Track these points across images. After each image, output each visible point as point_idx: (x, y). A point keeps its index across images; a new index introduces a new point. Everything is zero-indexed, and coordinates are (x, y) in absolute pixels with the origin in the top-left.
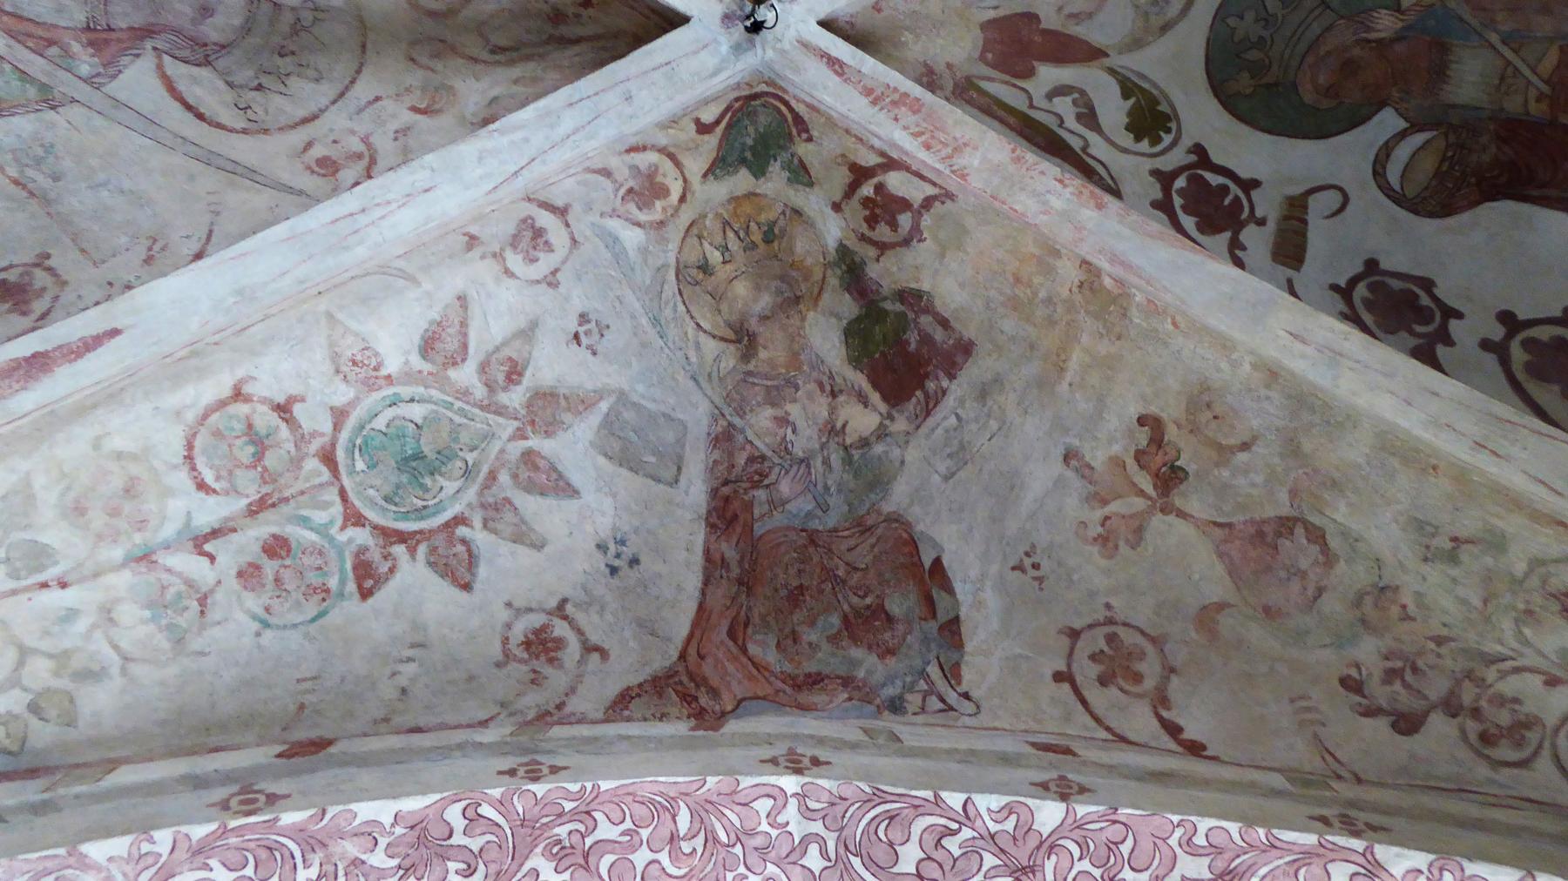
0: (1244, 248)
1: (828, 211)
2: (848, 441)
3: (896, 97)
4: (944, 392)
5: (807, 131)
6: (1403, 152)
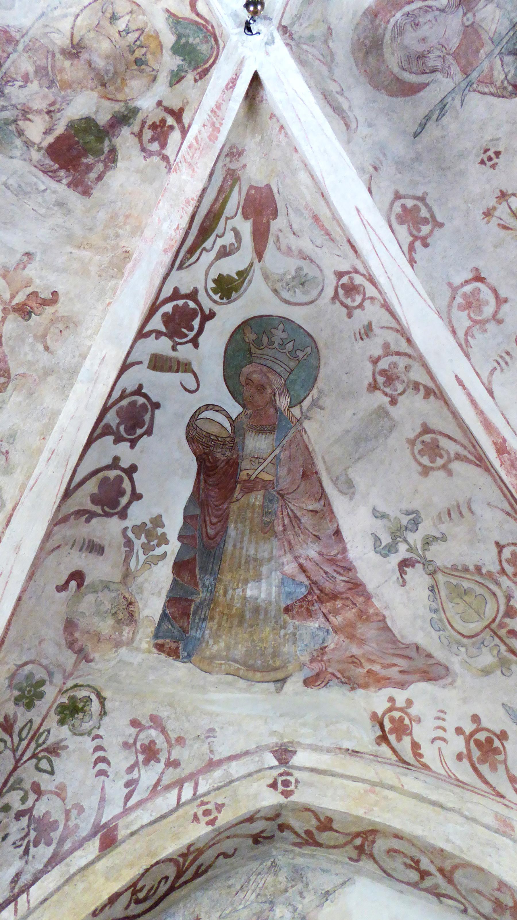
0: (157, 338)
1: (157, 99)
2: (20, 123)
3: (217, 125)
4: (59, 181)
5: (201, 78)
6: (219, 418)
